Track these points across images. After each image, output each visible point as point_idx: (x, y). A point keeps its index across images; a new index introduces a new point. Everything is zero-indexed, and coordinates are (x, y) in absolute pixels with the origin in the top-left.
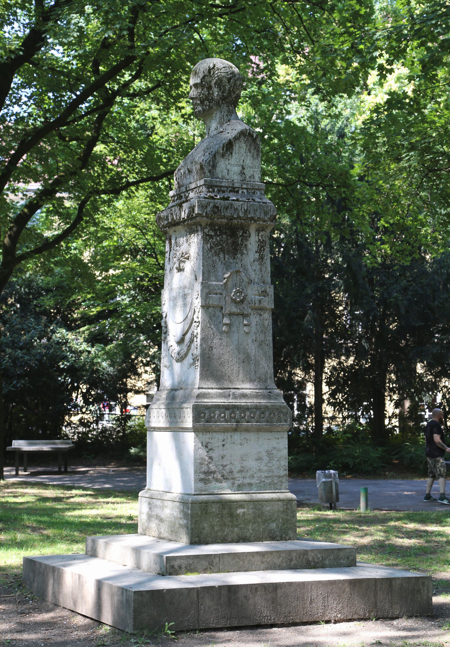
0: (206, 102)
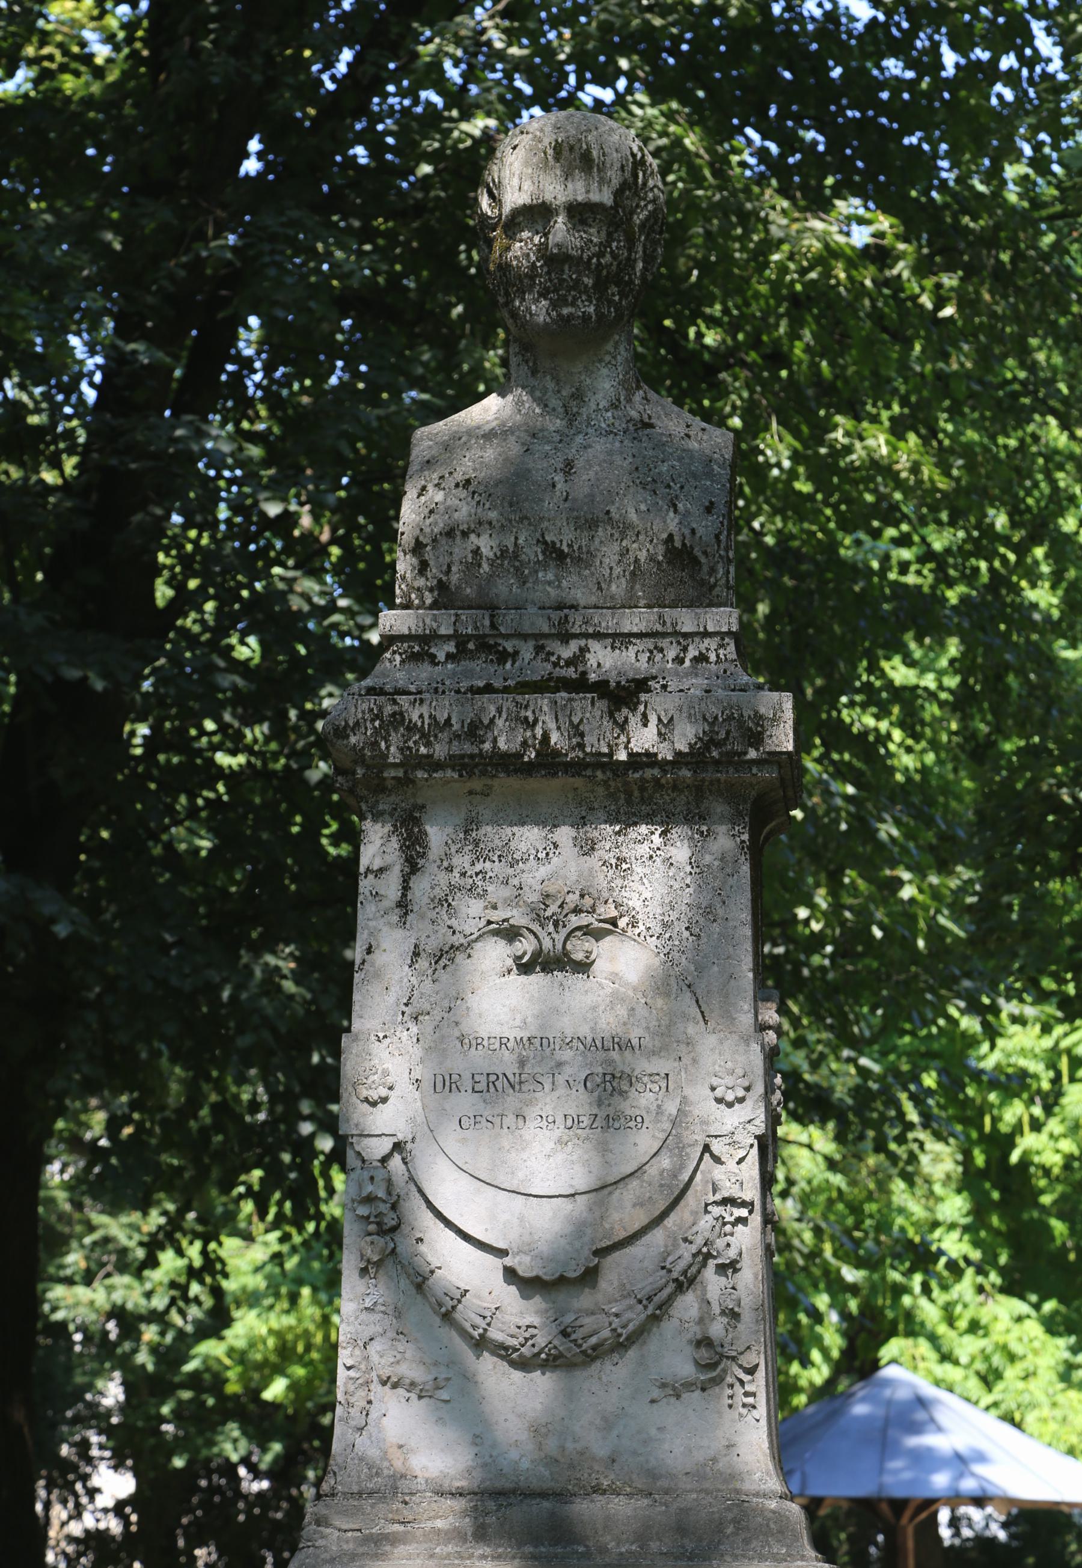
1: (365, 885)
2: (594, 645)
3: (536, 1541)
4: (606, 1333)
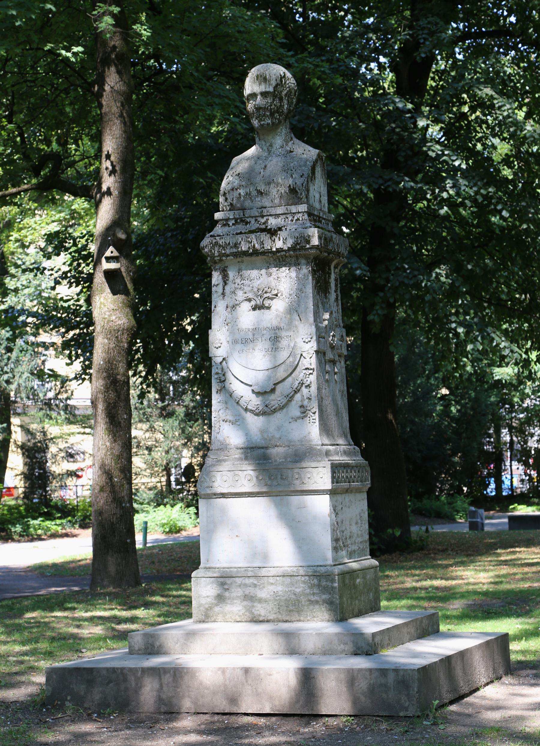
0: (276, 115)
1: (214, 289)
2: (270, 218)
3: (260, 460)
4: (277, 405)
